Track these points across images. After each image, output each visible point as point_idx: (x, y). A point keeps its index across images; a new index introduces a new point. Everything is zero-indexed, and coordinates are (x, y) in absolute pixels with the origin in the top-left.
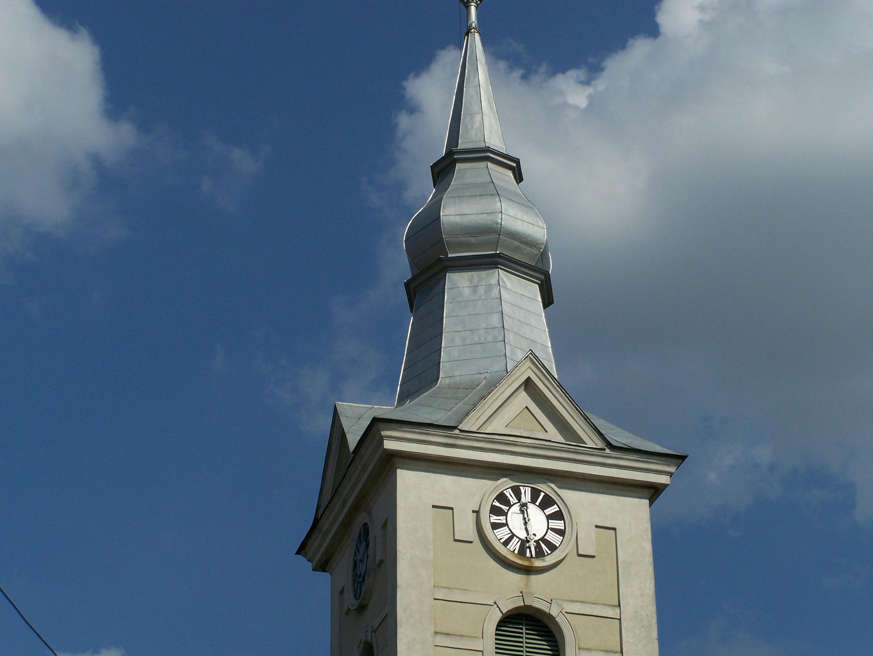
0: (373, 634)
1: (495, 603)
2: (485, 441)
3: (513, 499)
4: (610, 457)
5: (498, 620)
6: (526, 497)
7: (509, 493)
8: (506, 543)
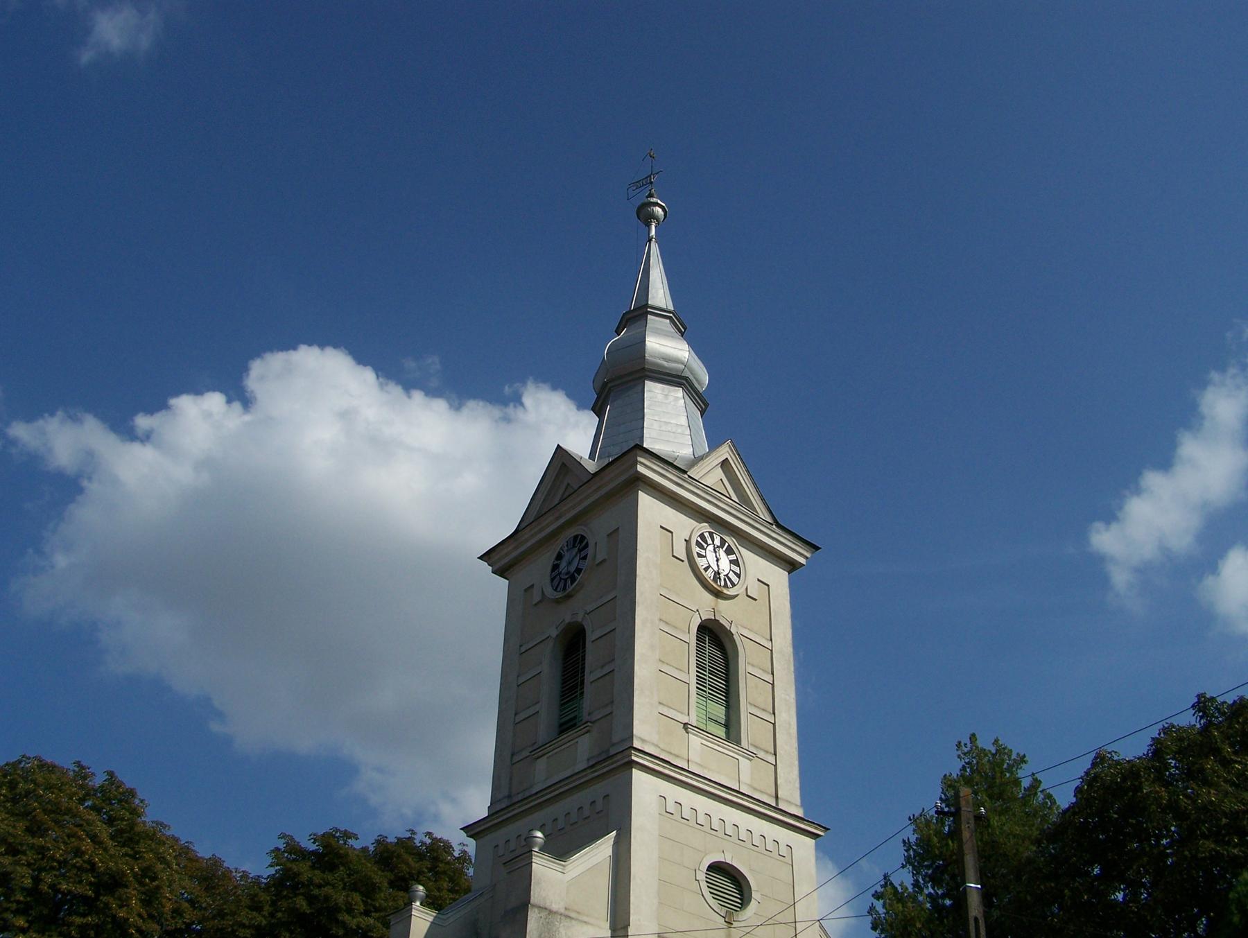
0: (716, 569)
1: (697, 610)
2: (702, 491)
3: (710, 541)
4: (774, 532)
5: (698, 624)
6: (717, 542)
7: (707, 535)
8: (706, 570)
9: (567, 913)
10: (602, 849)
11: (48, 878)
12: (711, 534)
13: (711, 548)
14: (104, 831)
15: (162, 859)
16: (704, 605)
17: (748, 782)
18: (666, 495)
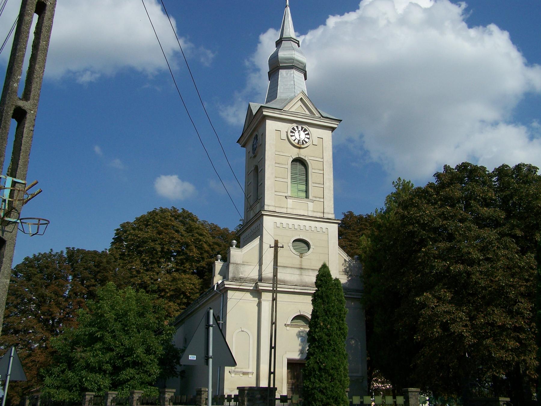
3: (296, 129)
9: (243, 263)
10: (256, 241)
11: (166, 247)
12: (297, 127)
13: (297, 132)
14: (182, 228)
15: (201, 235)
16: (295, 153)
17: (312, 210)
18: (276, 118)
